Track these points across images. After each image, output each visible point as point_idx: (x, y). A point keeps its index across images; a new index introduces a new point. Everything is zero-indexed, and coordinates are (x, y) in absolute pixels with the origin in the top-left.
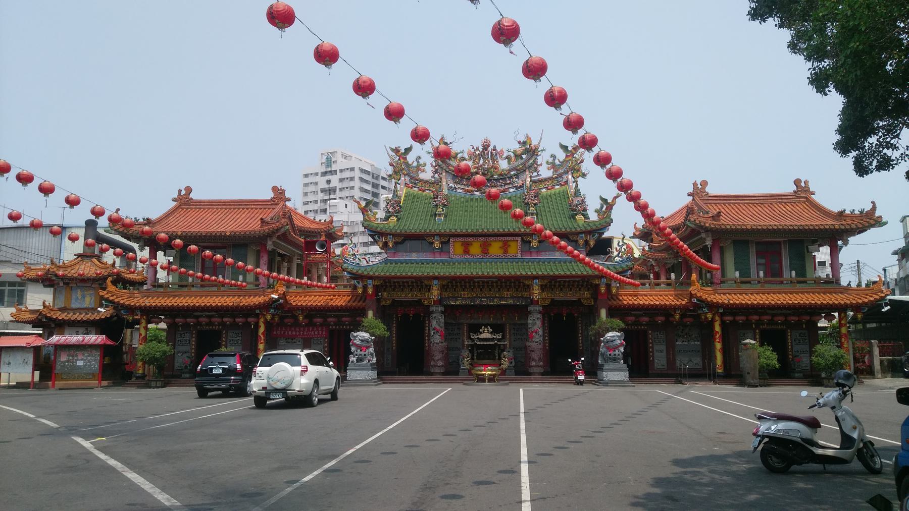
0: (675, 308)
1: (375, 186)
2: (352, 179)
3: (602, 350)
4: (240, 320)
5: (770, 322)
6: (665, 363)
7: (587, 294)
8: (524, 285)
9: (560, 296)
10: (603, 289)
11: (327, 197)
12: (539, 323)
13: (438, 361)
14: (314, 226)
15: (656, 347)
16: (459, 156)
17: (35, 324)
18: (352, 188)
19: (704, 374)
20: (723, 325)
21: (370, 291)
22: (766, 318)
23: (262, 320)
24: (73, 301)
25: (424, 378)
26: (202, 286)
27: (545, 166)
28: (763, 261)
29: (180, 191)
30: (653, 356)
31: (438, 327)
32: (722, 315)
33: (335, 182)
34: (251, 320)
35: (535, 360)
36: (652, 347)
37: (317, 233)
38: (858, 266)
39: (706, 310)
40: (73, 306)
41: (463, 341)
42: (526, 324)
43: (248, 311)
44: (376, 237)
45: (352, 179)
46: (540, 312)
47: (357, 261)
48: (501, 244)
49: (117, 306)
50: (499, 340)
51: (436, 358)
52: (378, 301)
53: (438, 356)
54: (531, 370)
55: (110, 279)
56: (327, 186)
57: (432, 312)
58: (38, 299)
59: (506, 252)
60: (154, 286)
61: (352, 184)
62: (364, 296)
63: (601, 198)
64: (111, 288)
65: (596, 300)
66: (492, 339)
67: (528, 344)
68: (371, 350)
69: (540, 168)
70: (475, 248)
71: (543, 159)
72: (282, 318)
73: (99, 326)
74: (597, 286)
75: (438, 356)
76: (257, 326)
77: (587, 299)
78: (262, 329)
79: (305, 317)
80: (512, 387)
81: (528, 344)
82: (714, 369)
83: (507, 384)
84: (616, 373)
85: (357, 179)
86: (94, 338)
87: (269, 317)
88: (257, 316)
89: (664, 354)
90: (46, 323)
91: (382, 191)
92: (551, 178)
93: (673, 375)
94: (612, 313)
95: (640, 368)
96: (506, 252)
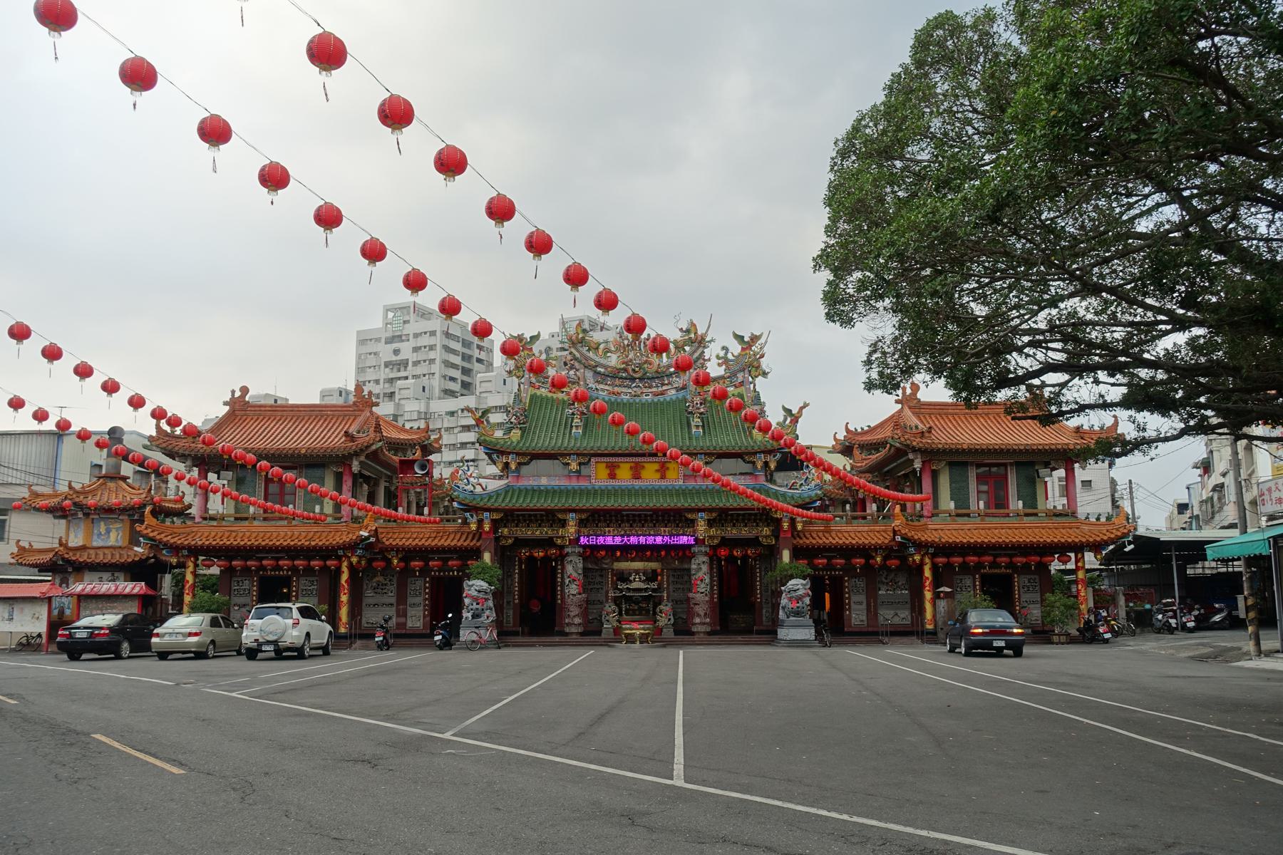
0: (876, 548)
1: (466, 358)
2: (432, 348)
3: (784, 601)
4: (316, 563)
5: (994, 565)
6: (864, 618)
7: (766, 531)
8: (687, 519)
9: (732, 532)
10: (786, 525)
11: (392, 375)
12: (705, 568)
13: (573, 619)
14: (403, 436)
15: (854, 598)
16: (602, 346)
17: (43, 568)
18: (432, 361)
19: (913, 632)
20: (935, 568)
21: (487, 527)
22: (987, 559)
23: (345, 564)
24: (95, 537)
25: (557, 639)
26: (265, 519)
27: (714, 361)
28: (985, 488)
29: (233, 392)
30: (849, 609)
31: (575, 575)
32: (933, 556)
33: (406, 351)
34: (331, 563)
35: (699, 615)
36: (849, 598)
37: (411, 445)
38: (1131, 488)
39: (912, 550)
40: (95, 544)
41: (607, 592)
42: (689, 570)
43: (327, 553)
44: (495, 456)
45: (432, 348)
46: (706, 554)
47: (470, 488)
48: (656, 466)
49: (156, 545)
50: (654, 590)
51: (572, 614)
52: (497, 539)
53: (574, 611)
54: (694, 629)
55: (148, 509)
56: (394, 358)
57: (567, 554)
58: (43, 534)
59: (663, 477)
60: (205, 519)
61: (432, 355)
62: (479, 533)
63: (784, 408)
64: (149, 520)
65: (777, 538)
66: (646, 590)
67: (691, 595)
68: (490, 603)
69: (708, 364)
70: (624, 472)
71: (712, 351)
72: (370, 561)
73: (134, 570)
74: (779, 521)
75: (574, 611)
76: (338, 571)
77: (766, 537)
78: (345, 577)
79: (400, 560)
80: (669, 651)
81: (691, 595)
82: (923, 626)
83: (664, 646)
84: (800, 630)
85: (438, 347)
86: (129, 587)
87: (354, 560)
88: (339, 558)
89: (864, 606)
90: (62, 566)
91: (477, 366)
92: (722, 377)
93: (872, 635)
94: (797, 553)
95: (832, 627)
96: (663, 477)
